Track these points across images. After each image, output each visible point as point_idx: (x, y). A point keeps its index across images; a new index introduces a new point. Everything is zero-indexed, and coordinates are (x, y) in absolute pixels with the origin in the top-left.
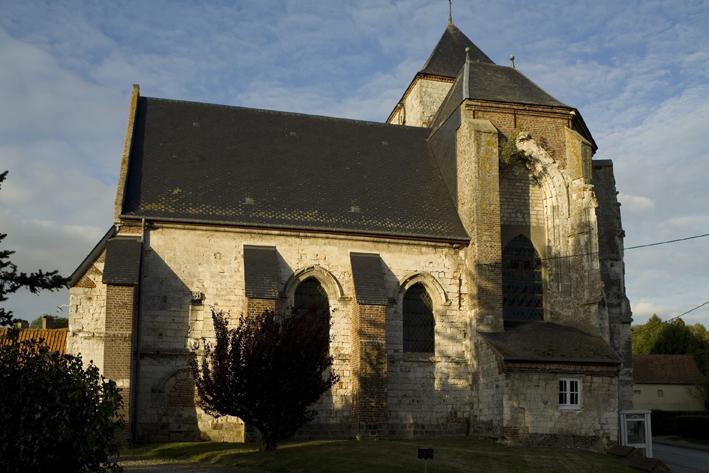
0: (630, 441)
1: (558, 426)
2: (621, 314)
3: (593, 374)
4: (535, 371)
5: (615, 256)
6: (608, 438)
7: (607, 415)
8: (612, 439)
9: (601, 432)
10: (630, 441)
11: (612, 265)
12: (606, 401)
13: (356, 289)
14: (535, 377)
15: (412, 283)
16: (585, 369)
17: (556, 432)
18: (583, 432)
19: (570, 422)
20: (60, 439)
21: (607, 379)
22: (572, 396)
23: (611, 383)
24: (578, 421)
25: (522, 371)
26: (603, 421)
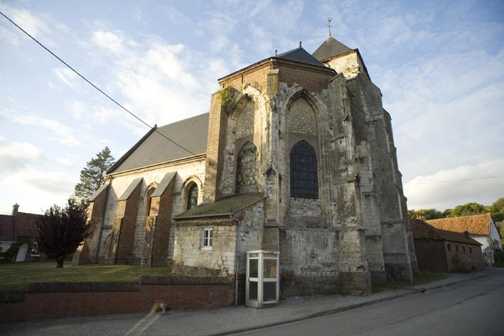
0: (275, 299)
1: (198, 261)
2: (348, 176)
3: (218, 224)
4: (188, 224)
5: (342, 135)
6: (227, 271)
7: (227, 254)
8: (229, 272)
9: (223, 267)
10: (275, 299)
11: (341, 142)
12: (227, 244)
13: (218, 158)
14: (189, 229)
15: (189, 182)
16: (213, 221)
17: (196, 266)
18: (212, 266)
19: (205, 259)
20: (313, 94)
21: (228, 228)
22: (207, 236)
23: (230, 230)
24: (209, 259)
25: (183, 225)
26: (224, 258)
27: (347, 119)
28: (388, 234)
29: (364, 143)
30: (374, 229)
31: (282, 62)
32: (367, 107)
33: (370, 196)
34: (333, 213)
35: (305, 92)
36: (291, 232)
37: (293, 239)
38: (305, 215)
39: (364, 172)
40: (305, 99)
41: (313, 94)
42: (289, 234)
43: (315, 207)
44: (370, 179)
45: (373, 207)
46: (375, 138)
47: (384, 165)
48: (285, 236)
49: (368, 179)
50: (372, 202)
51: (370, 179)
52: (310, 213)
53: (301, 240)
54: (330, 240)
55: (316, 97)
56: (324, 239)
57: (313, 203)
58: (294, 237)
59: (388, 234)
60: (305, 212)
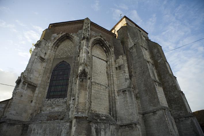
27: (89, 46)
28: (154, 121)
29: (121, 56)
30: (131, 117)
31: (78, 21)
32: (132, 39)
33: (125, 91)
34: (71, 106)
35: (68, 35)
36: (33, 126)
37: (32, 132)
38: (53, 110)
39: (121, 75)
40: (69, 39)
41: (71, 34)
42: (30, 128)
43: (61, 104)
44: (126, 79)
45: (129, 99)
46: (136, 54)
47: (144, 68)
48: (27, 130)
49: (124, 79)
50: (128, 95)
51: (126, 79)
52: (56, 109)
53: (39, 132)
54: (63, 131)
55: (73, 35)
56: (59, 130)
57: (61, 100)
58: (34, 130)
59: (154, 121)
60: (53, 108)
